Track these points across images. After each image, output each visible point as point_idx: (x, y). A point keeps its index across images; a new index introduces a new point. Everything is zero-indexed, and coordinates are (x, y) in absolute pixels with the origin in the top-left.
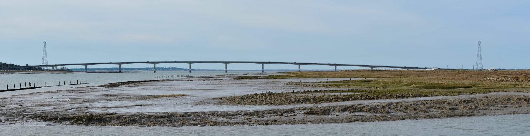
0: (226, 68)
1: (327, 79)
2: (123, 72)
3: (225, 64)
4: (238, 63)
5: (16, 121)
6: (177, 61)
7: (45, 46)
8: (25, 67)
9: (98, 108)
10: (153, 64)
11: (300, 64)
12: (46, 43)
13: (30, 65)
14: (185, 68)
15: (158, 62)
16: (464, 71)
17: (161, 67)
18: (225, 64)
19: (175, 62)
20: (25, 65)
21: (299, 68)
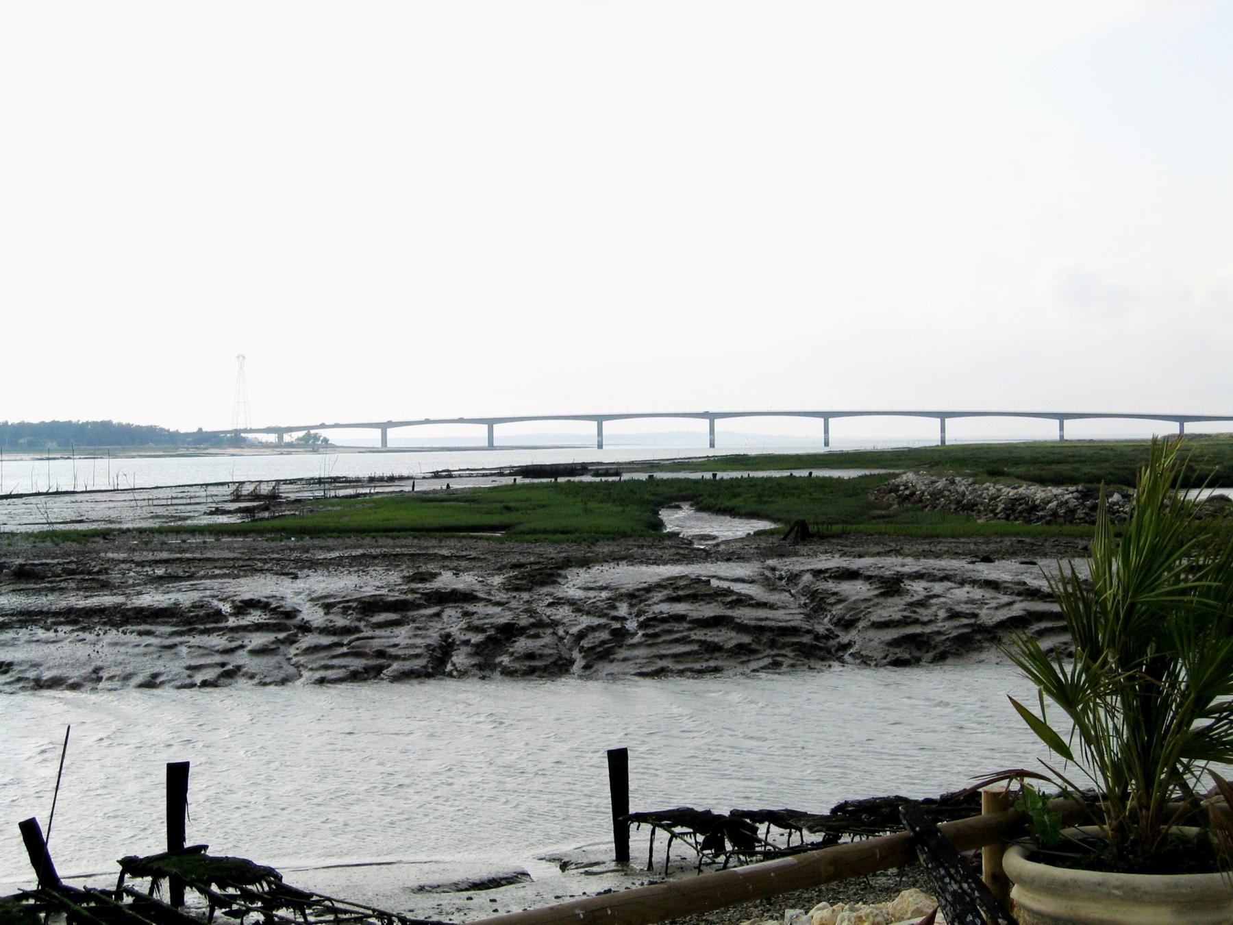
0: (826, 431)
1: (712, 445)
2: (269, 430)
3: (821, 420)
4: (351, 422)
5: (190, 611)
6: (432, 418)
7: (241, 368)
8: (194, 433)
9: (895, 724)
10: (596, 423)
11: (1062, 417)
12: (244, 358)
13: (209, 430)
14: (185, 425)
15: (609, 416)
16: (1206, 435)
17: (17, 421)
18: (1178, 423)
19: (427, 421)
20: (195, 430)
21: (1062, 428)
